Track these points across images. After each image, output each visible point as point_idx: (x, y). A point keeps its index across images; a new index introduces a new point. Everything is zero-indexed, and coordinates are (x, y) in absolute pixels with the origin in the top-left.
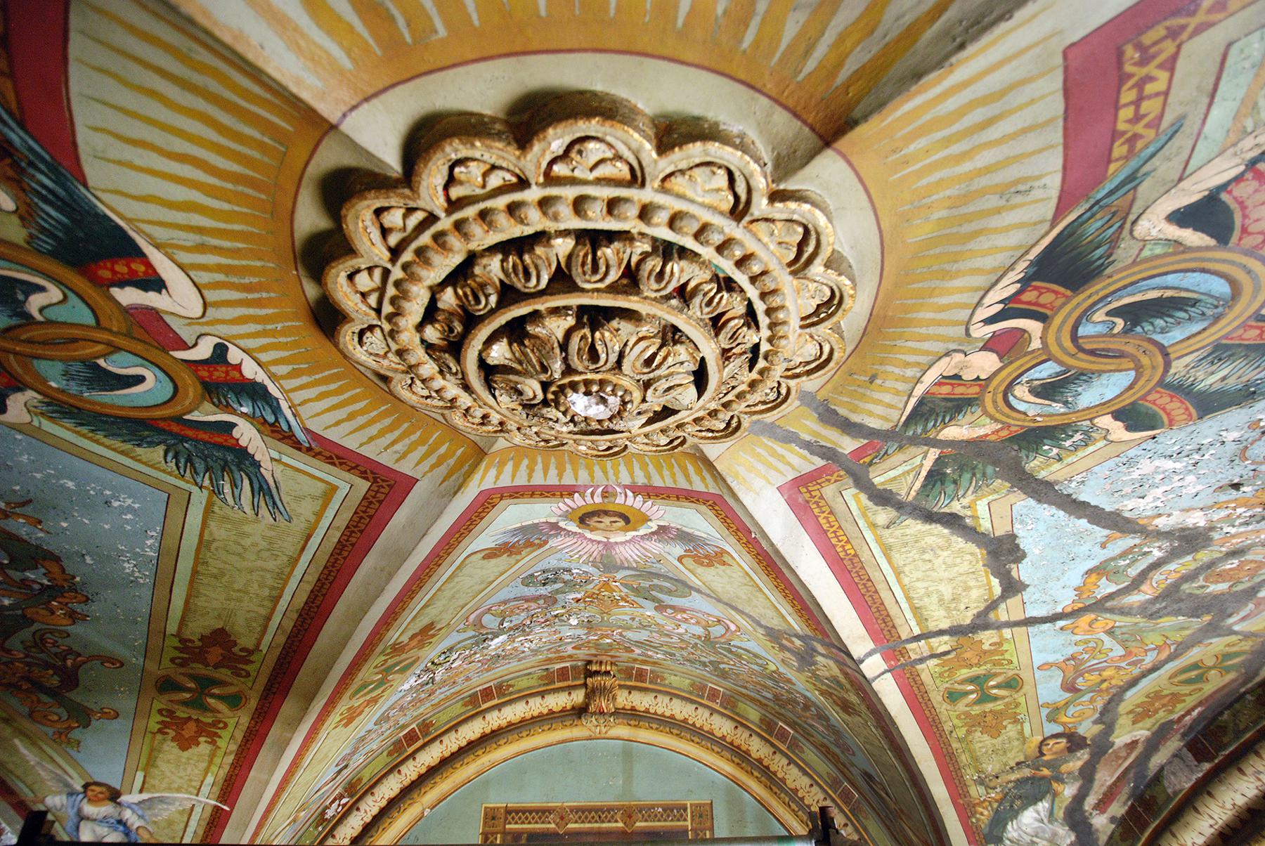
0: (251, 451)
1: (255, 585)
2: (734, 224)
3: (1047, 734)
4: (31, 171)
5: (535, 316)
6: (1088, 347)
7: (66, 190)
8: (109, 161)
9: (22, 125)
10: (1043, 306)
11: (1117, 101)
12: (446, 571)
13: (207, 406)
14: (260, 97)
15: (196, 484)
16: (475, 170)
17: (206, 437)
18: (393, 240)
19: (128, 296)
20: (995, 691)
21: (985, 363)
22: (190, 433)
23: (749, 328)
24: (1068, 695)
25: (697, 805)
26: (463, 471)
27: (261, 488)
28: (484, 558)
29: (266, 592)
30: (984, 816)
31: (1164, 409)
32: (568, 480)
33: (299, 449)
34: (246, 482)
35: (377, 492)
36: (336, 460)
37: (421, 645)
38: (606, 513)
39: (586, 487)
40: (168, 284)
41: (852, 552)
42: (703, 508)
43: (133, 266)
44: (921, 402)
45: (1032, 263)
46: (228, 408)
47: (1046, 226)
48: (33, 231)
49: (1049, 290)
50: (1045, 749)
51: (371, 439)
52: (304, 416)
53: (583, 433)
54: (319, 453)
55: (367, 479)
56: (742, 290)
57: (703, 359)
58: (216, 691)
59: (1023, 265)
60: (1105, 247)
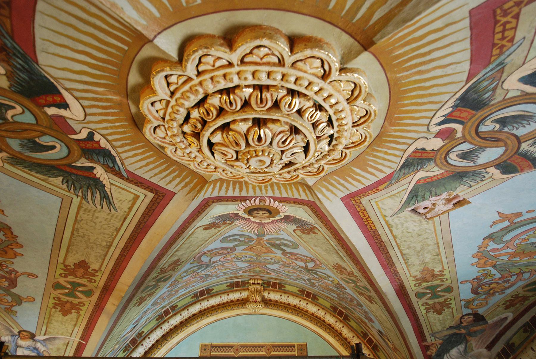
0: (101, 179)
1: (100, 241)
2: (323, 82)
3: (464, 314)
4: (14, 57)
5: (234, 121)
6: (483, 136)
7: (28, 65)
8: (49, 53)
9: (12, 38)
10: (462, 118)
11: (494, 31)
12: (186, 234)
13: (83, 160)
14: (118, 28)
15: (76, 195)
16: (210, 60)
17: (81, 173)
18: (172, 88)
19: (52, 111)
20: (440, 293)
21: (437, 143)
22: (75, 171)
23: (329, 127)
24: (474, 296)
25: (299, 345)
26: (197, 189)
27: (105, 197)
28: (204, 229)
29: (104, 244)
30: (433, 351)
31: (519, 165)
32: (244, 194)
33: (123, 179)
34: (98, 194)
35: (157, 198)
36: (139, 185)
37: (173, 269)
38: (261, 209)
39: (253, 197)
40: (70, 106)
41: (374, 228)
42: (306, 208)
43: (55, 98)
44: (406, 161)
45: (457, 99)
46: (92, 160)
47: (464, 83)
48: (12, 83)
49: (465, 111)
50: (462, 320)
51: (155, 175)
52: (126, 164)
53: (253, 173)
54: (132, 181)
55: (153, 193)
56: (326, 111)
57: (308, 141)
58: (80, 289)
59: (453, 100)
60: (490, 93)
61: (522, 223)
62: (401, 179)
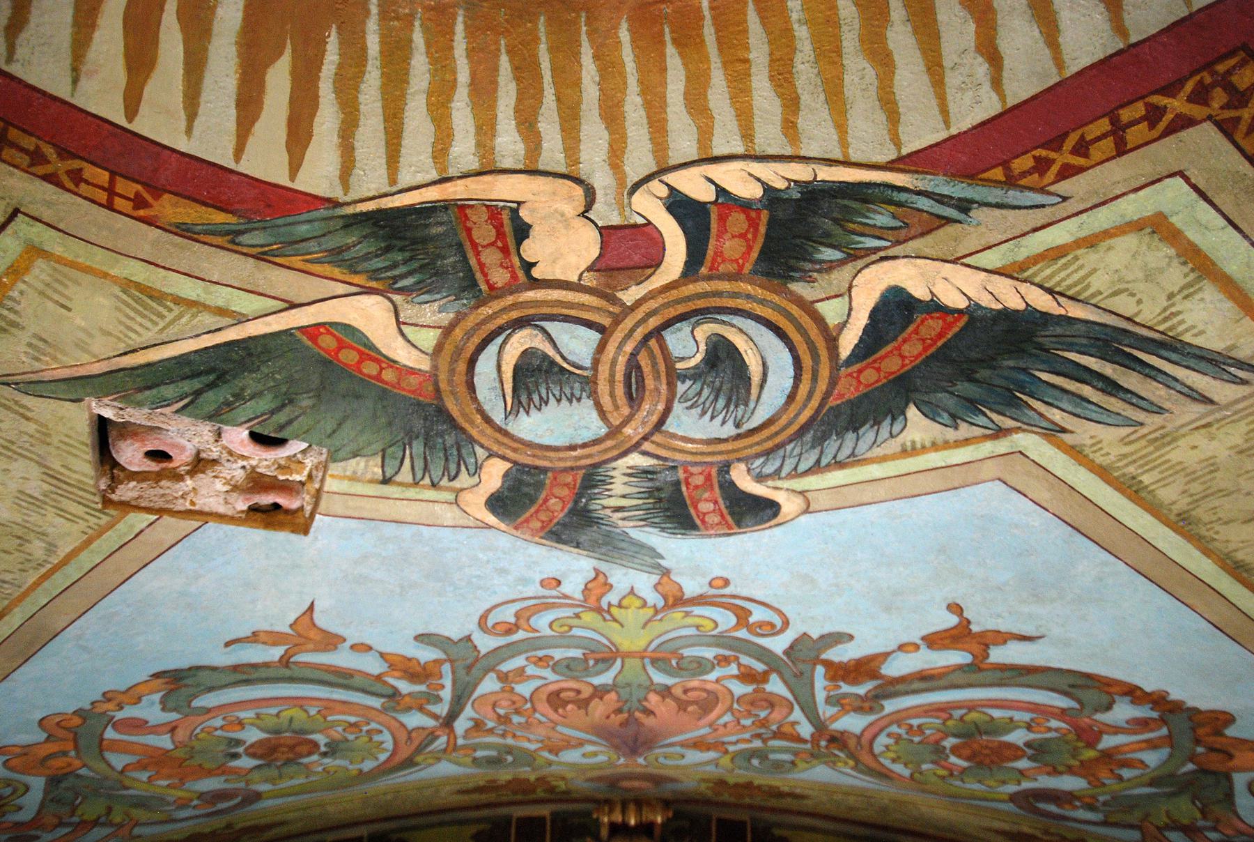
61: (308, 673)
62: (296, 261)
